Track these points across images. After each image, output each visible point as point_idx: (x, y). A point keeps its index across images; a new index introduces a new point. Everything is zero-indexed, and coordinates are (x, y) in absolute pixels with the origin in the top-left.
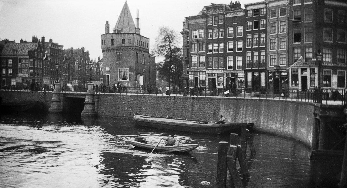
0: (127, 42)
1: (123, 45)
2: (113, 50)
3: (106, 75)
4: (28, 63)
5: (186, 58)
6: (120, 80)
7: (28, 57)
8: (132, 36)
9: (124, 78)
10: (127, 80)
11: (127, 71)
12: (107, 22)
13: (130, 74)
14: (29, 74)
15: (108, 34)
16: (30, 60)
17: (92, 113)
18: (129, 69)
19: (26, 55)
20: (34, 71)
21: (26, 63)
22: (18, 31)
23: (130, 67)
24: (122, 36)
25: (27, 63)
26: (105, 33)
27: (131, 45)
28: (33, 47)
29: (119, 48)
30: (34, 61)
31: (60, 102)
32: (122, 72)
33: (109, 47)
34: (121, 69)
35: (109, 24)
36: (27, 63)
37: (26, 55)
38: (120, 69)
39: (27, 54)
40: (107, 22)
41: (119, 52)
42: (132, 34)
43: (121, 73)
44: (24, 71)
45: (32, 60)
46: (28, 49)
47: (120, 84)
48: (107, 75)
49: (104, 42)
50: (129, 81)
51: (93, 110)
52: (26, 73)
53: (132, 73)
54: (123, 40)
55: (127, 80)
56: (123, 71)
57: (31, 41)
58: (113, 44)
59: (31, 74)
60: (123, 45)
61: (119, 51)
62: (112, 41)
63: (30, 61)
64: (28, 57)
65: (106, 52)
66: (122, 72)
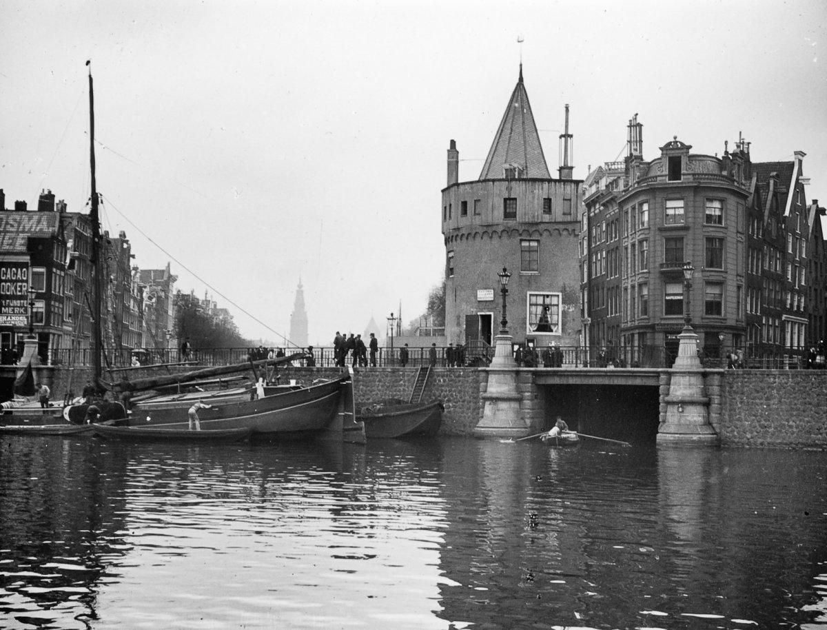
0: (558, 207)
1: (547, 218)
2: (509, 232)
3: (479, 313)
4: (27, 281)
5: (662, 266)
6: (530, 331)
7: (27, 259)
8: (574, 192)
9: (544, 326)
10: (552, 331)
11: (554, 301)
12: (453, 143)
13: (564, 312)
14: (27, 317)
15: (565, 182)
16: (36, 270)
17: (705, 435)
18: (560, 294)
19: (21, 254)
20: (48, 306)
21: (17, 281)
22: (42, 172)
23: (563, 290)
24: (542, 188)
25: (22, 281)
26: (477, 179)
27: (568, 218)
28: (44, 227)
29: (532, 229)
30: (49, 273)
31: (519, 400)
32: (536, 305)
33: (496, 222)
34: (533, 295)
35: (458, 147)
36: (22, 281)
37: (21, 254)
38: (530, 295)
39: (24, 248)
40: (453, 143)
41: (529, 241)
42: (573, 185)
43: (534, 308)
44: (9, 306)
45: (42, 270)
46: (23, 232)
47: (531, 345)
48: (482, 316)
49: (448, 208)
50: (560, 333)
51: (708, 423)
52: (20, 314)
53: (571, 310)
54: (548, 202)
55: (552, 331)
56: (540, 300)
57: (13, 208)
58: (509, 215)
59: (35, 317)
60: (547, 218)
61: (530, 235)
62: (509, 201)
63: (34, 274)
64: (27, 259)
65: (456, 240)
66: (536, 305)
